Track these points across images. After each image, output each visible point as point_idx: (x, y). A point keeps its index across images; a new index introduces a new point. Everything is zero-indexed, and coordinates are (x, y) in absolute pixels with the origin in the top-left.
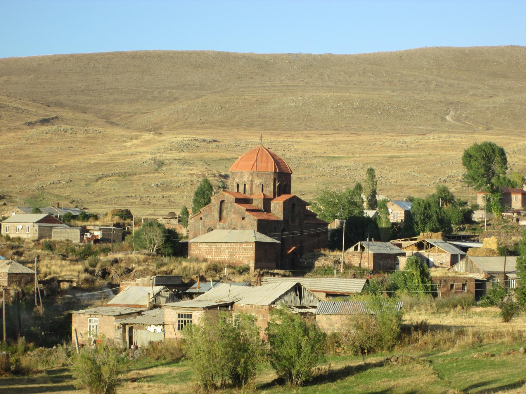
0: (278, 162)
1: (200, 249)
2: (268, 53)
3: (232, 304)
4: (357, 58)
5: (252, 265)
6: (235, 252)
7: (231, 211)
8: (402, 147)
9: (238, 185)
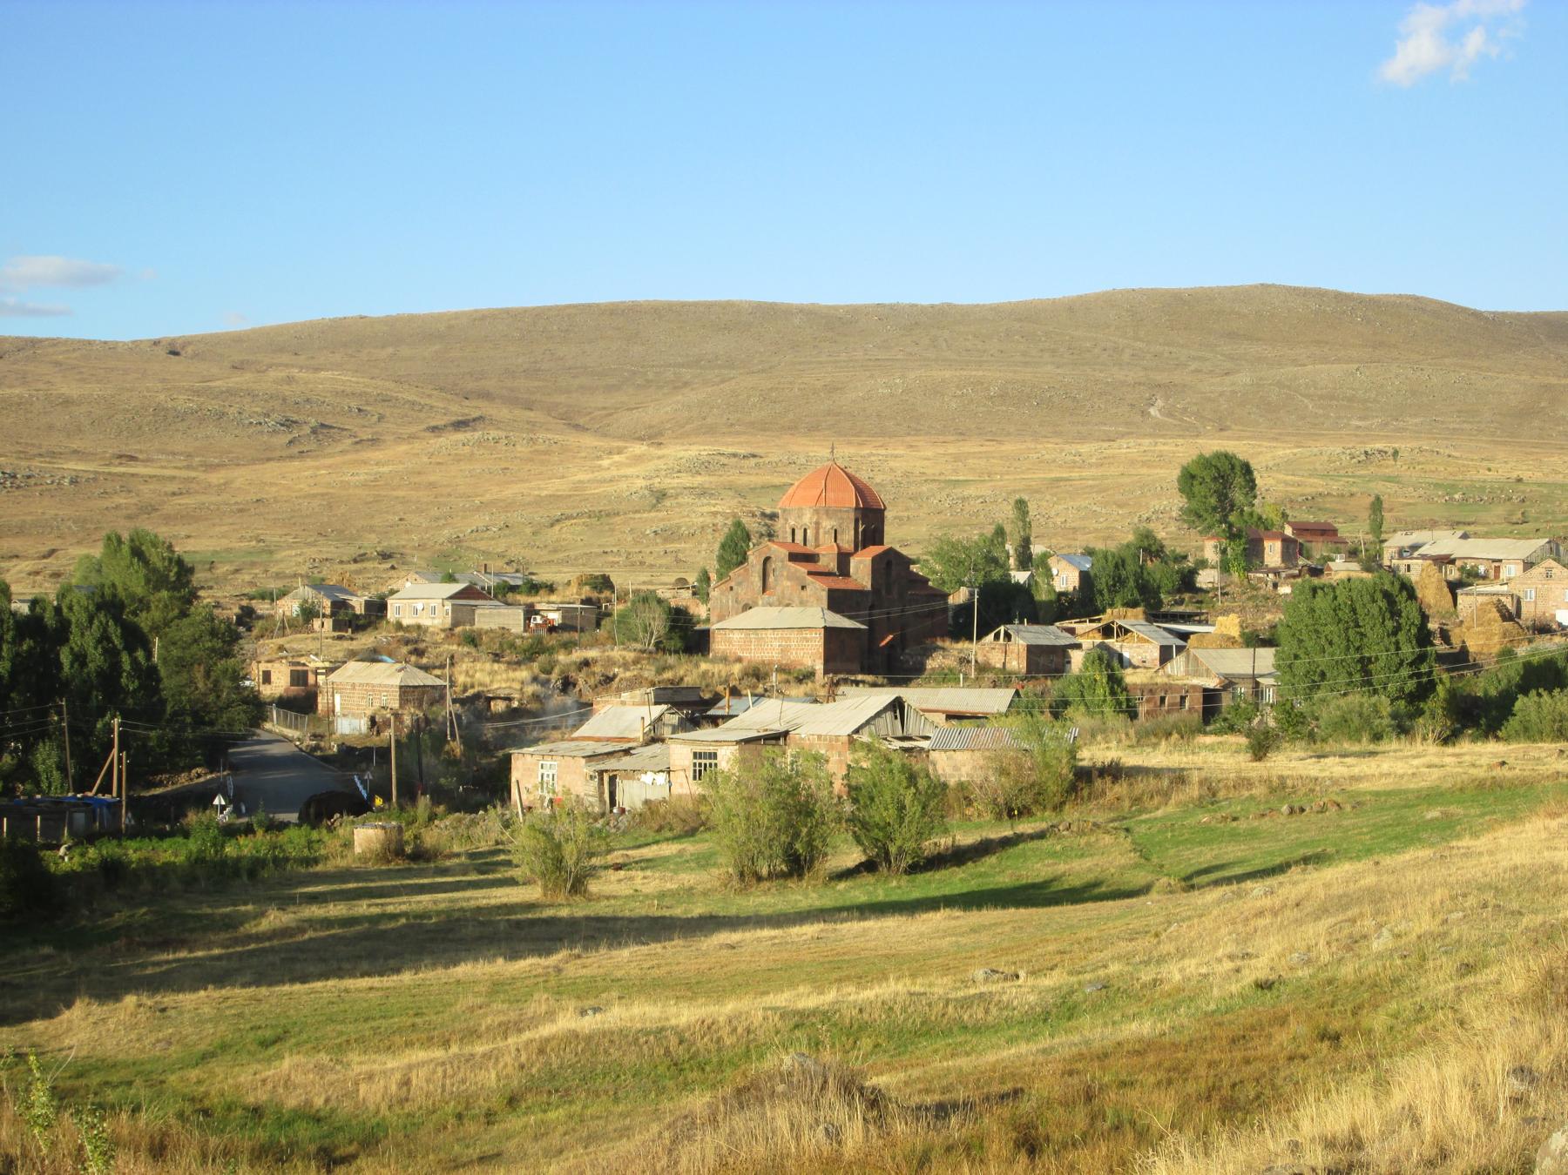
0: (861, 491)
1: (730, 641)
3: (786, 734)
5: (819, 667)
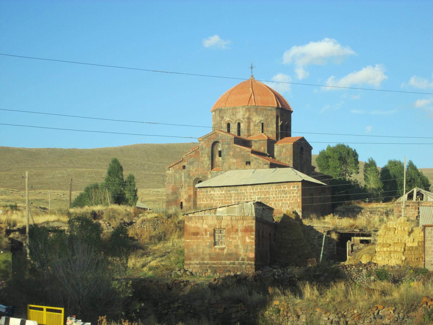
0: (278, 97)
2: (34, 148)
4: (93, 150)
6: (269, 198)
7: (229, 155)
8: (158, 194)
9: (229, 125)
